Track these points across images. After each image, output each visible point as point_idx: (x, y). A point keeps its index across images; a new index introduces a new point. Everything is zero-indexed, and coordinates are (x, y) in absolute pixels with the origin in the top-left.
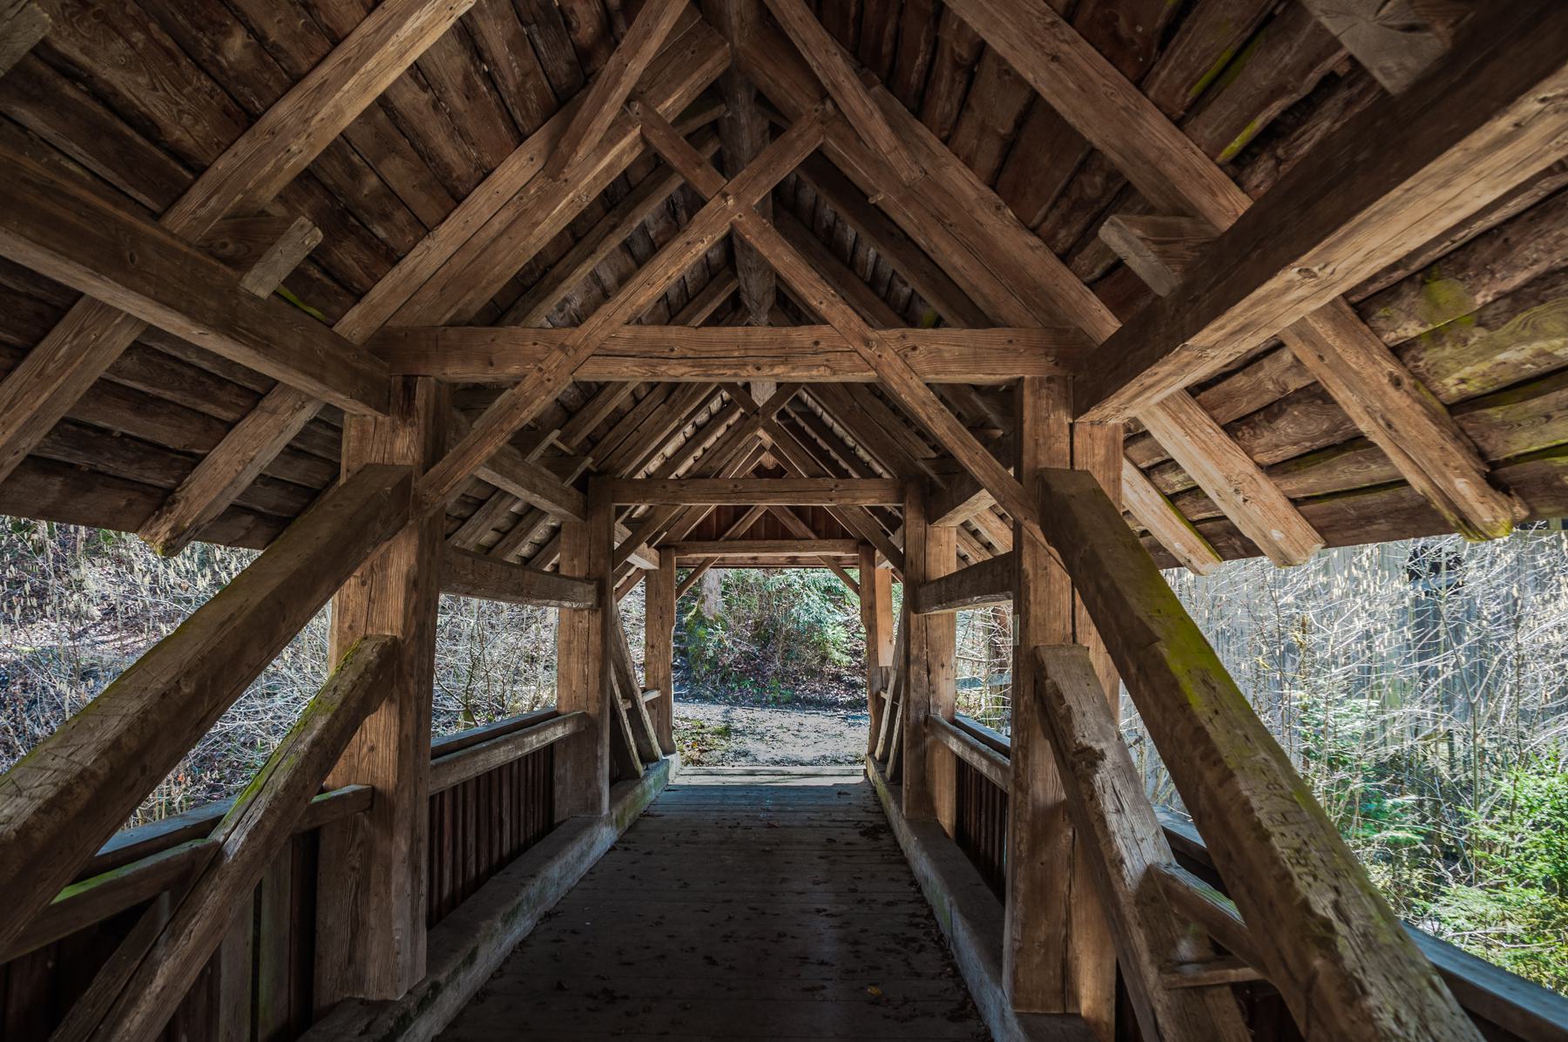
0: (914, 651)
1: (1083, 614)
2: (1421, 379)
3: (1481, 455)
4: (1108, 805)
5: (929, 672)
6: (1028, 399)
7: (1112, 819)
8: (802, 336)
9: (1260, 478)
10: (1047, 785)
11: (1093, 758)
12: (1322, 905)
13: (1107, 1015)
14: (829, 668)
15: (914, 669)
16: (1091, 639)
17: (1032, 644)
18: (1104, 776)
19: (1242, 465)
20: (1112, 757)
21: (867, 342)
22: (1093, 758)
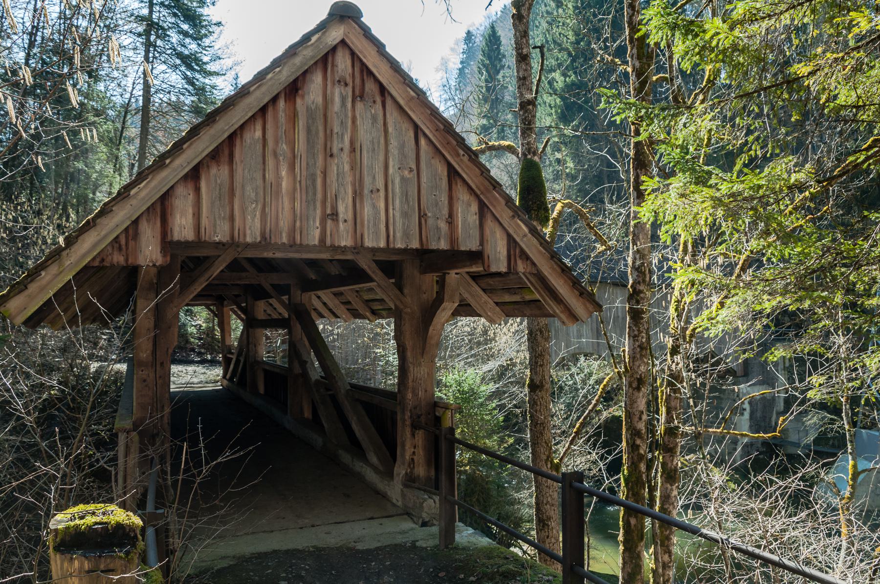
0: (251, 340)
1: (303, 334)
2: (361, 296)
3: (371, 309)
4: (309, 370)
5: (255, 346)
6: (292, 288)
7: (310, 372)
8: (244, 274)
9: (341, 305)
10: (297, 370)
11: (306, 362)
12: (335, 375)
13: (311, 417)
14: (189, 346)
15: (250, 346)
16: (305, 339)
17: (114, 209)
18: (308, 365)
19: (337, 302)
20: (309, 362)
21: (258, 276)
22: (306, 362)
